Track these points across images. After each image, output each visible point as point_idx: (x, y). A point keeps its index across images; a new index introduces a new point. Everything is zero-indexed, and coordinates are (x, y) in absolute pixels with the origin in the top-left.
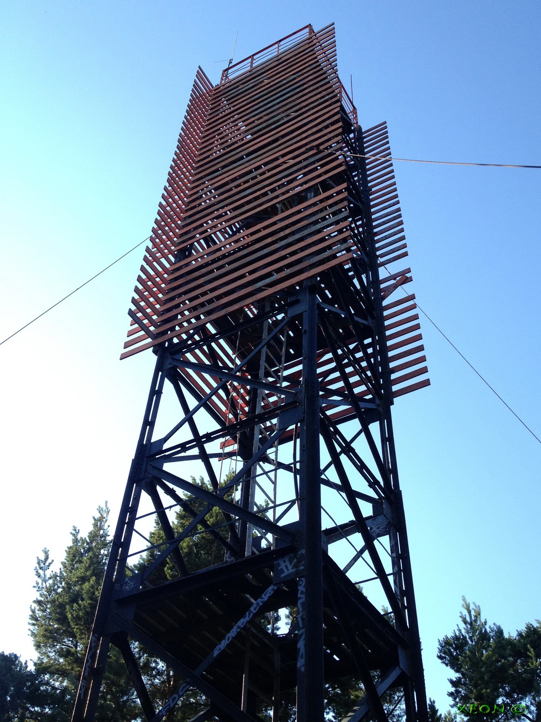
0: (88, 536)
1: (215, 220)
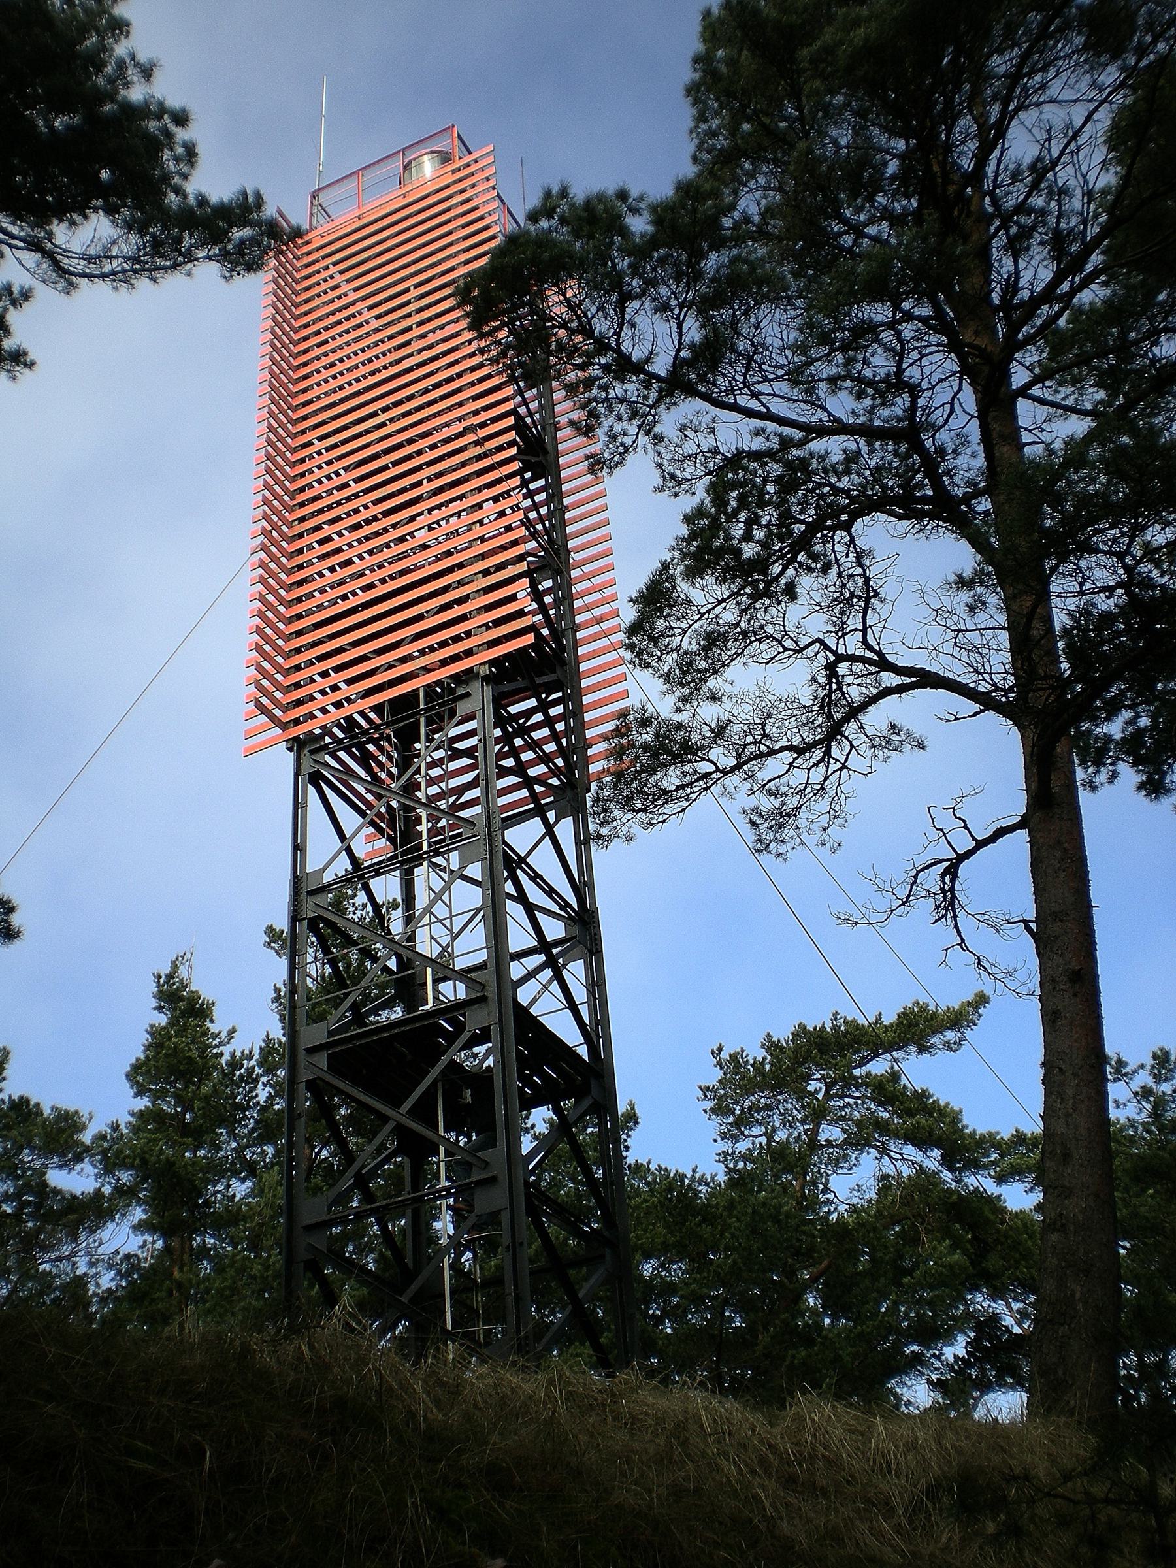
1: (355, 936)
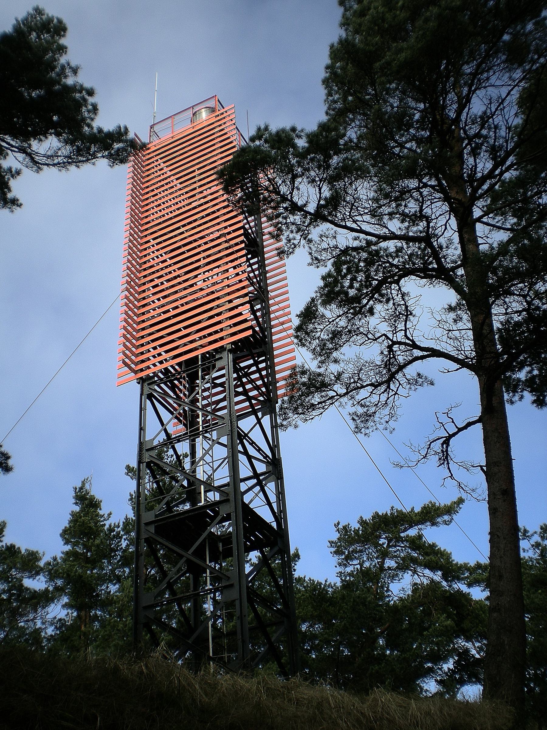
0: (59, 619)
